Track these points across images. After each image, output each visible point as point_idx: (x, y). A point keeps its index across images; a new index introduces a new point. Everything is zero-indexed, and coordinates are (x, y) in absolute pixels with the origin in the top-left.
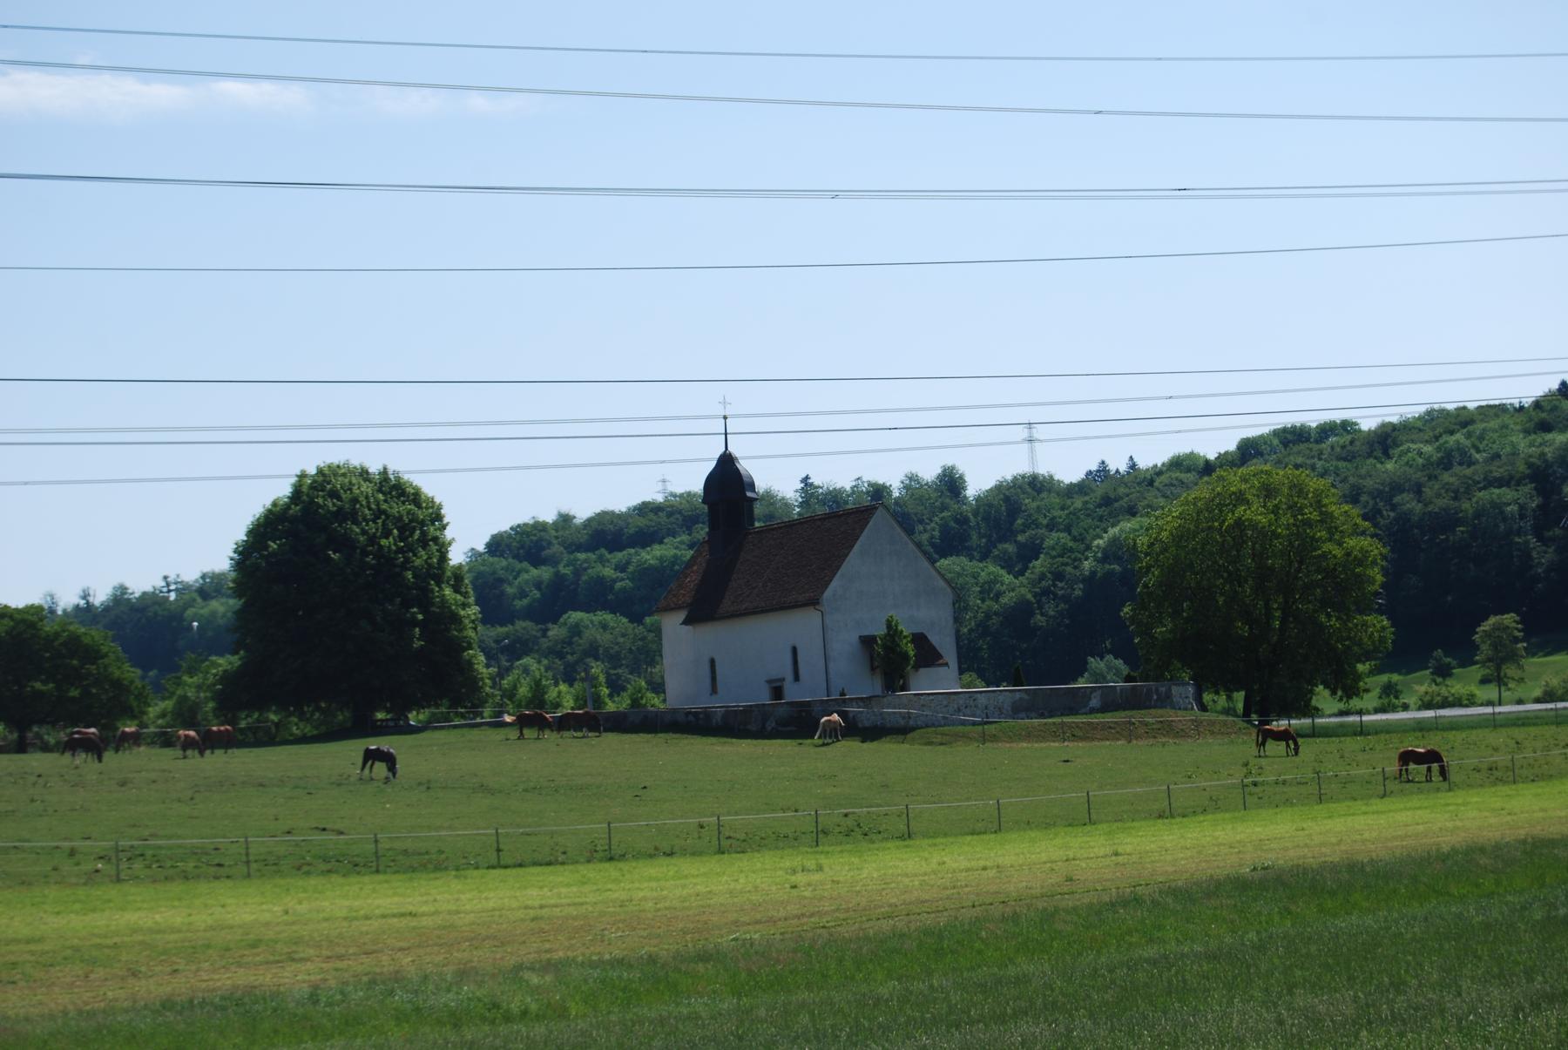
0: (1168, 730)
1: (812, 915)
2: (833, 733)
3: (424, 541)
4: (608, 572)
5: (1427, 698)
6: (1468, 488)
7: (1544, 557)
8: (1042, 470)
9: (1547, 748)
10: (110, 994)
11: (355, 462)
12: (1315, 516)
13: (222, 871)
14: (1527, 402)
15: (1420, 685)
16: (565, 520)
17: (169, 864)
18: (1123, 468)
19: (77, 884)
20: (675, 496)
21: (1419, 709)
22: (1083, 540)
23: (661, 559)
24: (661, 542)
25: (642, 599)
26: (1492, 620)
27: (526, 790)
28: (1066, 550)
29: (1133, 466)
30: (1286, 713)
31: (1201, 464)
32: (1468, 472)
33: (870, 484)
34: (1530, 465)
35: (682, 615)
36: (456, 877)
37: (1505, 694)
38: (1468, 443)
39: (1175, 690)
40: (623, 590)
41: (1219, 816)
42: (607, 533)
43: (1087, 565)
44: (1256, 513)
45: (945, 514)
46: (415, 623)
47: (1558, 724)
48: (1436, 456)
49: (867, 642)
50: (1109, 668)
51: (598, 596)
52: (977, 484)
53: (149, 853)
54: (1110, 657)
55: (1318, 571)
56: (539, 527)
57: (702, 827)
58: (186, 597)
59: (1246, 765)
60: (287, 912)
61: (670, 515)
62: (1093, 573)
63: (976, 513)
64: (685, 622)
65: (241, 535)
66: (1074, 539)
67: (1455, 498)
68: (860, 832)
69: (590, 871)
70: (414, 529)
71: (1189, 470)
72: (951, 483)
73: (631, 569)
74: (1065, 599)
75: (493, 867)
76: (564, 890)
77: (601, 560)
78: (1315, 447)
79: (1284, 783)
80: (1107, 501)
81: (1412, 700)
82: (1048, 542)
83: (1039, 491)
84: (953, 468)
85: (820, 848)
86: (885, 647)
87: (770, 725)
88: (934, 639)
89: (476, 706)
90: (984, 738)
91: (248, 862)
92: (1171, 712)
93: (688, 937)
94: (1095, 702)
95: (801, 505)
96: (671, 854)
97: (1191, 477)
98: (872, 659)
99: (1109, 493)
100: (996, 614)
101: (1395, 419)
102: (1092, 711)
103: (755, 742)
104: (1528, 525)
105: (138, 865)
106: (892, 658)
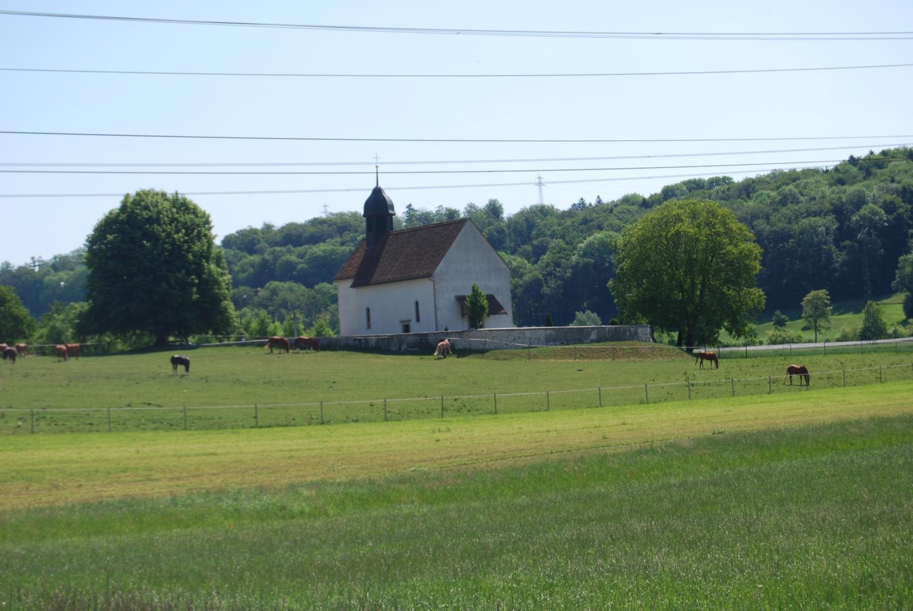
0: (636, 353)
1: (456, 457)
2: (445, 353)
3: (199, 236)
4: (293, 258)
5: (774, 338)
6: (797, 216)
7: (840, 257)
8: (547, 202)
9: (859, 367)
10: (43, 499)
11: (158, 189)
12: (722, 230)
13: (93, 427)
14: (830, 168)
15: (769, 330)
16: (268, 228)
17: (61, 423)
18: (594, 203)
19: (8, 434)
20: (333, 214)
21: (769, 344)
22: (572, 244)
23: (324, 251)
24: (324, 242)
25: (326, 270)
26: (813, 293)
27: (264, 383)
28: (562, 250)
29: (599, 201)
30: (704, 342)
31: (641, 200)
32: (796, 207)
33: (447, 209)
34: (832, 204)
35: (350, 282)
36: (232, 433)
37: (819, 336)
38: (796, 190)
39: (640, 330)
40: (303, 269)
41: (676, 403)
42: (293, 236)
43: (574, 258)
44: (687, 227)
45: (491, 227)
46: (193, 285)
47: (863, 353)
48: (778, 198)
49: (460, 299)
50: (589, 318)
51: (288, 273)
52: (510, 210)
53: (48, 416)
54: (589, 312)
55: (723, 262)
56: (253, 232)
57: (372, 405)
58: (45, 270)
59: (685, 374)
60: (138, 452)
61: (330, 225)
62: (578, 264)
63: (509, 227)
64: (353, 286)
65: (90, 231)
66: (567, 243)
67: (789, 223)
68: (467, 409)
69: (313, 430)
70: (194, 229)
71: (633, 204)
72: (494, 209)
73: (307, 257)
74: (561, 278)
75: (254, 427)
76: (299, 441)
77: (289, 251)
78: (707, 191)
79: (709, 384)
80: (586, 221)
81: (765, 339)
82: (552, 245)
83: (545, 215)
84: (496, 200)
85: (444, 419)
86: (471, 303)
87: (404, 347)
88: (499, 298)
89: (228, 335)
90: (530, 357)
91: (109, 422)
92: (638, 343)
93: (385, 469)
94: (593, 336)
95: (406, 221)
96: (357, 421)
97: (634, 208)
98: (462, 309)
99: (586, 217)
100: (520, 286)
101: (753, 176)
102: (592, 341)
103: (395, 357)
104: (830, 238)
105: (42, 424)
106: (475, 309)
